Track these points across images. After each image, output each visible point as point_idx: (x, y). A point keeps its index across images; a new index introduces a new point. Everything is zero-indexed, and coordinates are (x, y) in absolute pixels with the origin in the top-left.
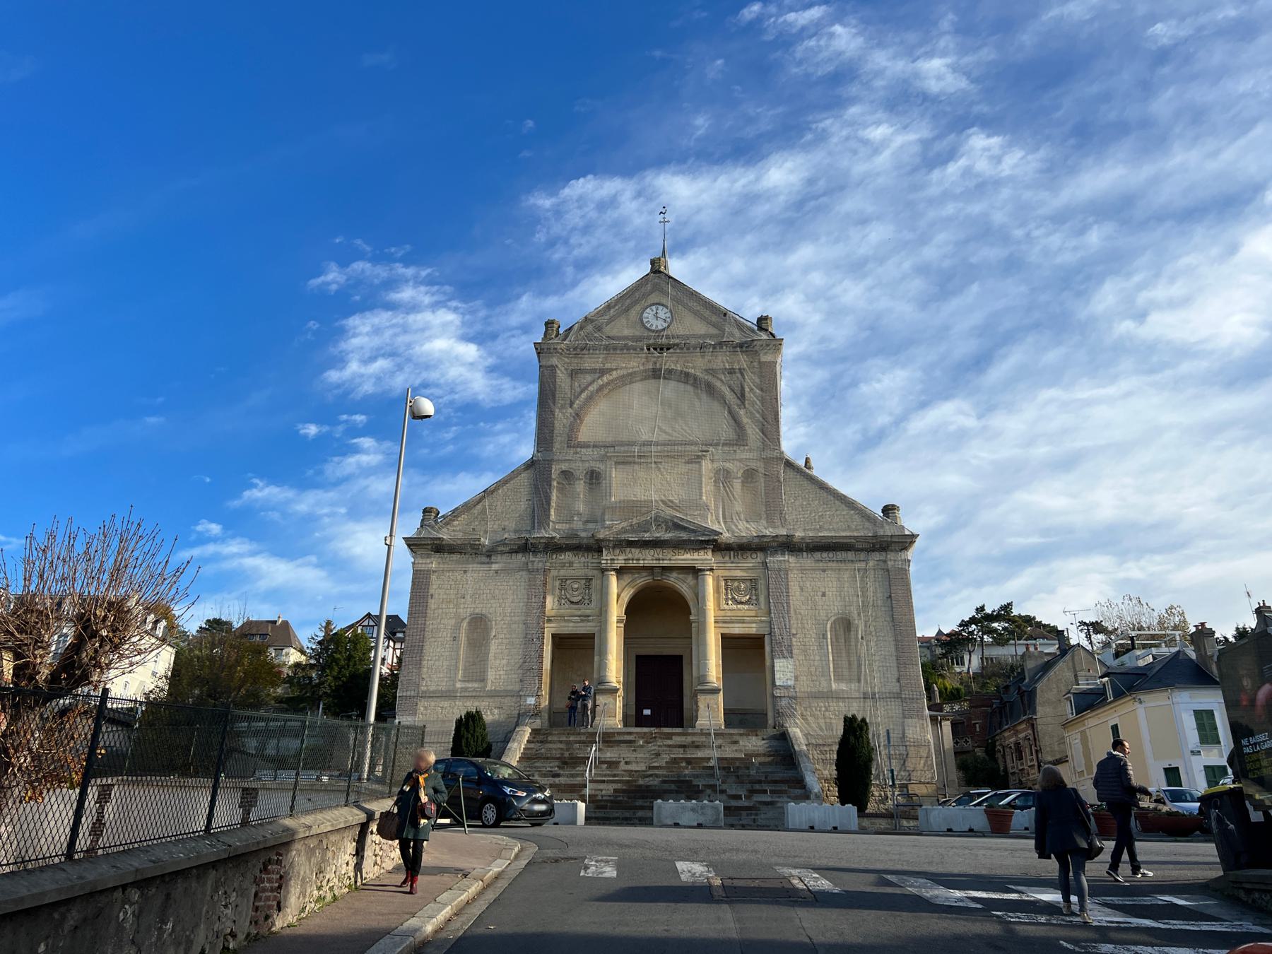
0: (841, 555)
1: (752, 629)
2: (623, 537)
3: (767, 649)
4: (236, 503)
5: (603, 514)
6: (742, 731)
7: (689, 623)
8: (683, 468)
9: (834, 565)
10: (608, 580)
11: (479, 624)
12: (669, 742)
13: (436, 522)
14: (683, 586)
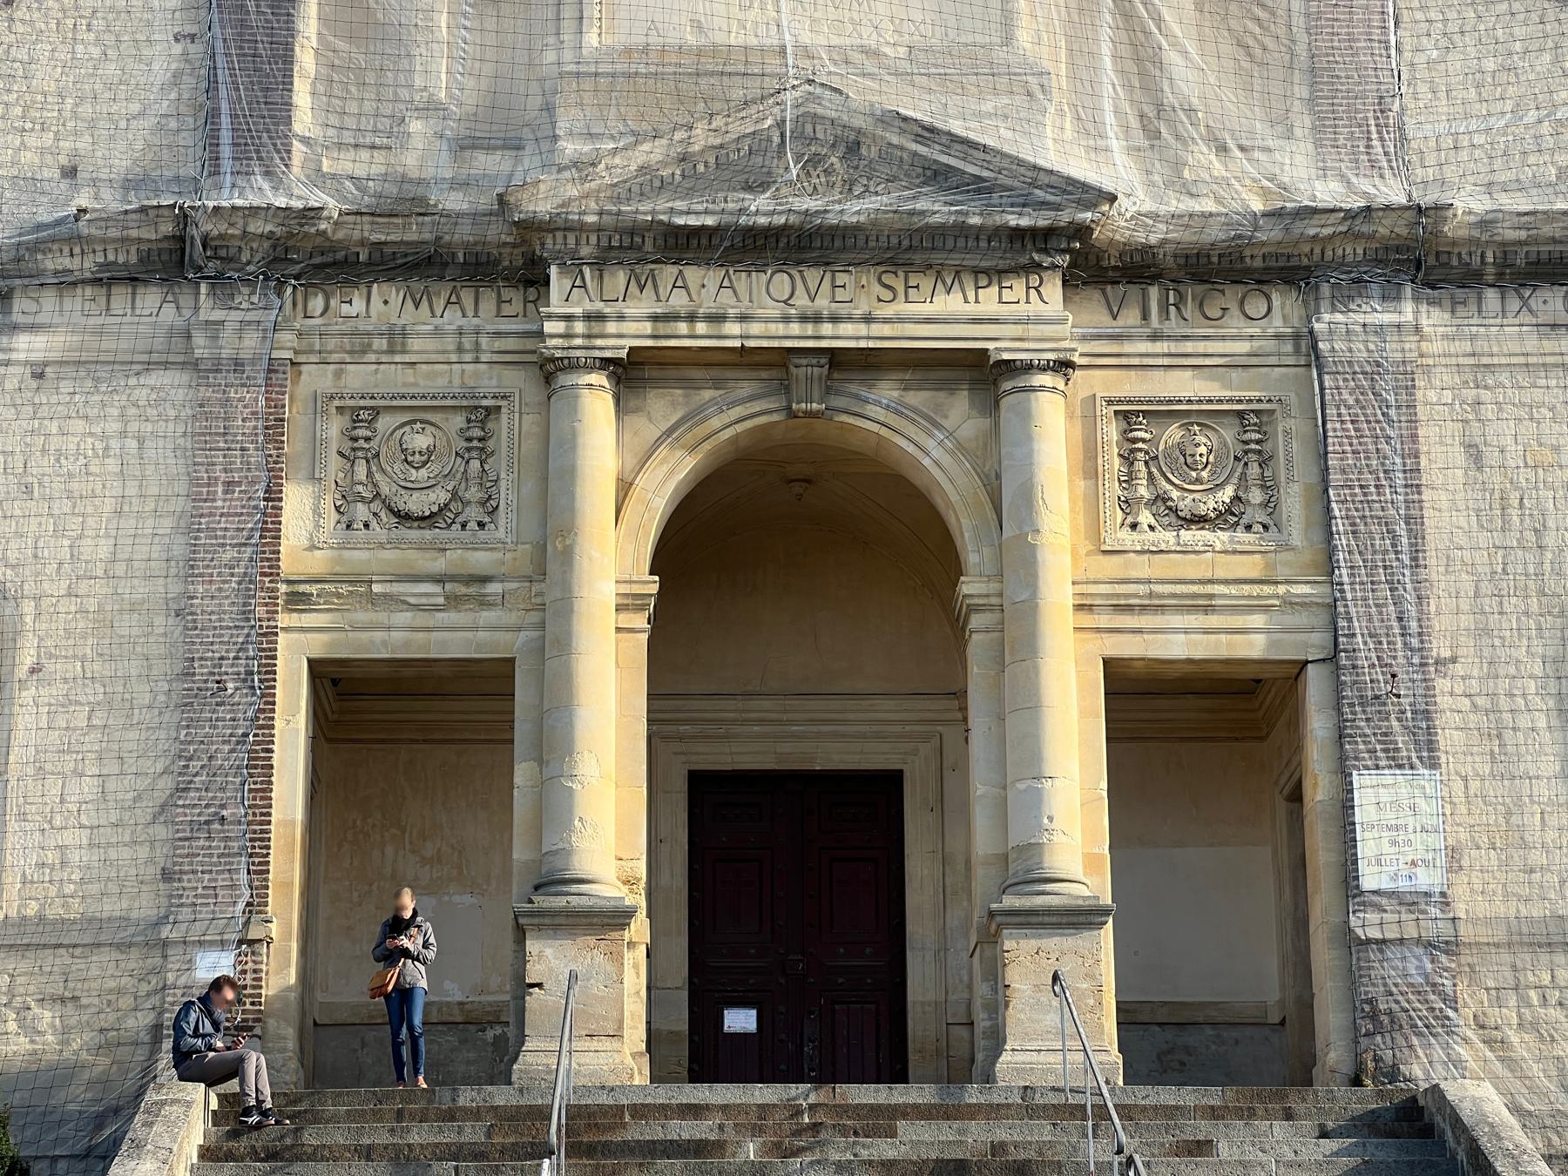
1: (1248, 640)
2: (646, 210)
3: (1318, 725)
6: (1213, 1096)
7: (955, 624)
14: (925, 439)
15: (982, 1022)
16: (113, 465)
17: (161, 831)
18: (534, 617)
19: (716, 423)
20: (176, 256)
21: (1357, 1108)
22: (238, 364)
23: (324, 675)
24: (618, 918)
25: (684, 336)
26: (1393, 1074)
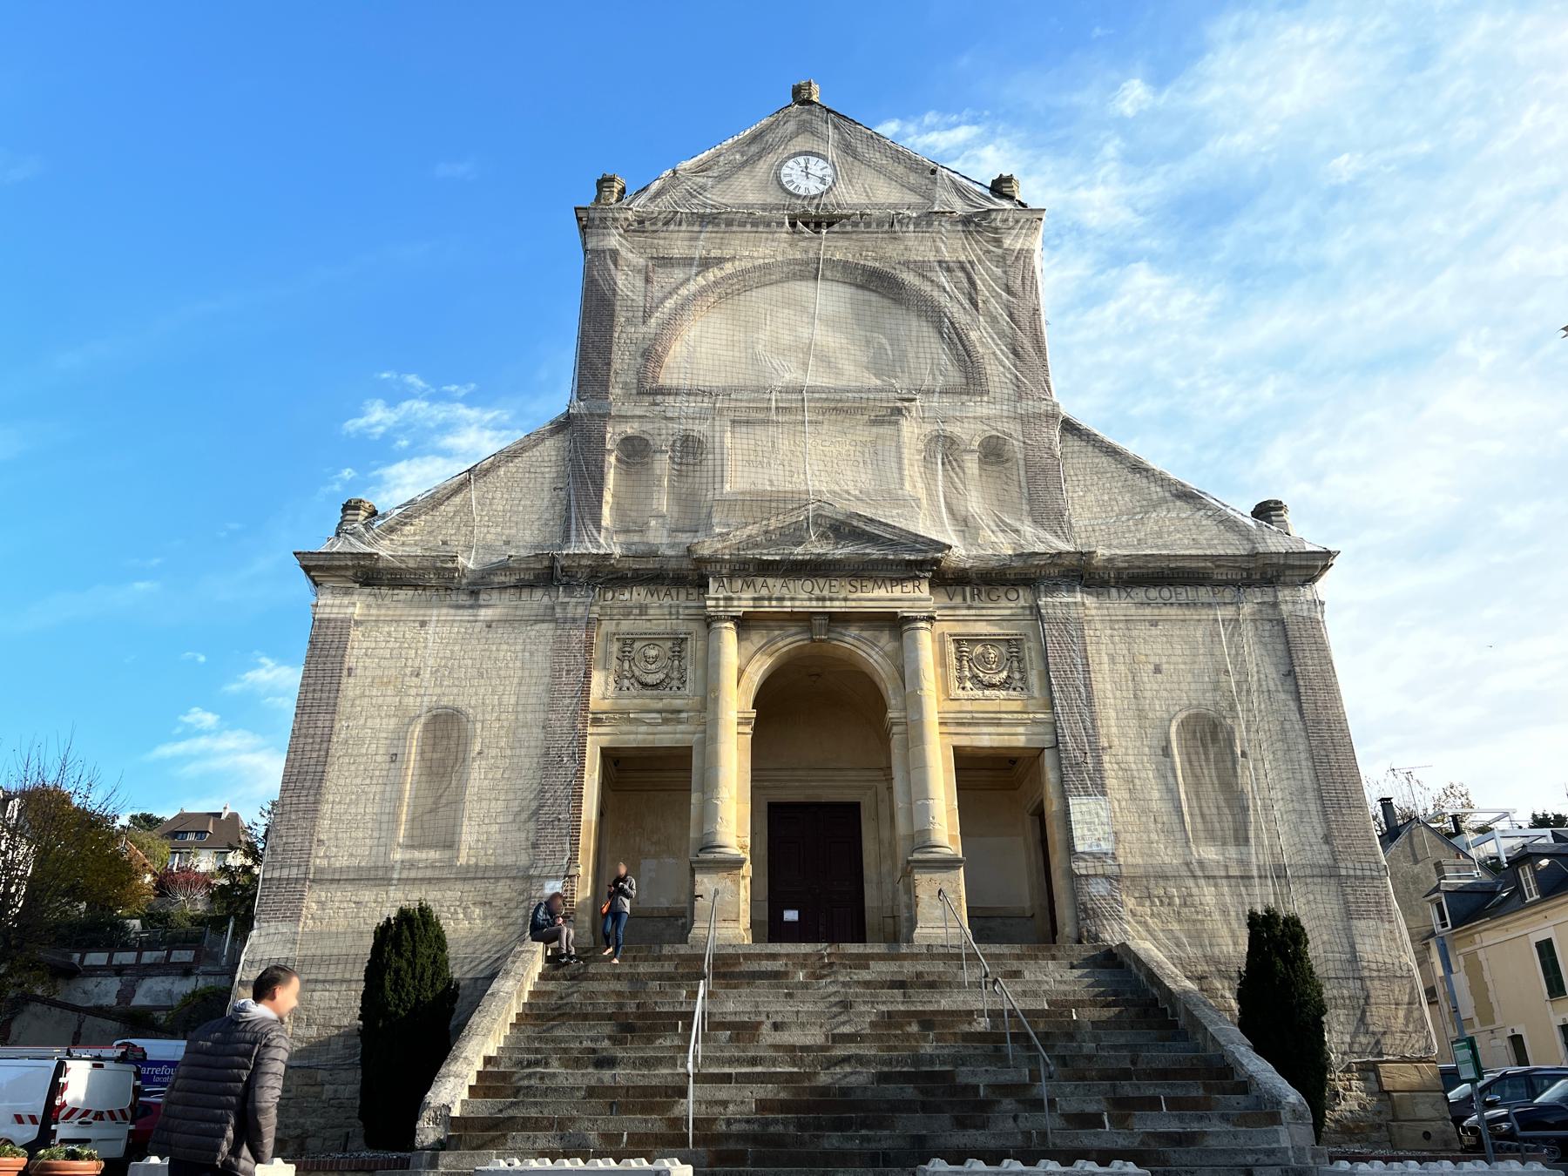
0: (1186, 594)
1: (1018, 738)
2: (750, 554)
3: (1051, 776)
4: (234, 688)
5: (709, 515)
6: (1016, 949)
7: (885, 739)
8: (865, 433)
9: (1173, 612)
10: (719, 638)
11: (446, 731)
12: (865, 975)
13: (367, 527)
14: (872, 652)
15: (904, 914)
16: (518, 664)
17: (532, 825)
18: (701, 728)
19: (780, 644)
20: (547, 575)
21: (1086, 954)
22: (574, 620)
23: (608, 755)
24: (738, 863)
25: (767, 607)
26: (1096, 938)
